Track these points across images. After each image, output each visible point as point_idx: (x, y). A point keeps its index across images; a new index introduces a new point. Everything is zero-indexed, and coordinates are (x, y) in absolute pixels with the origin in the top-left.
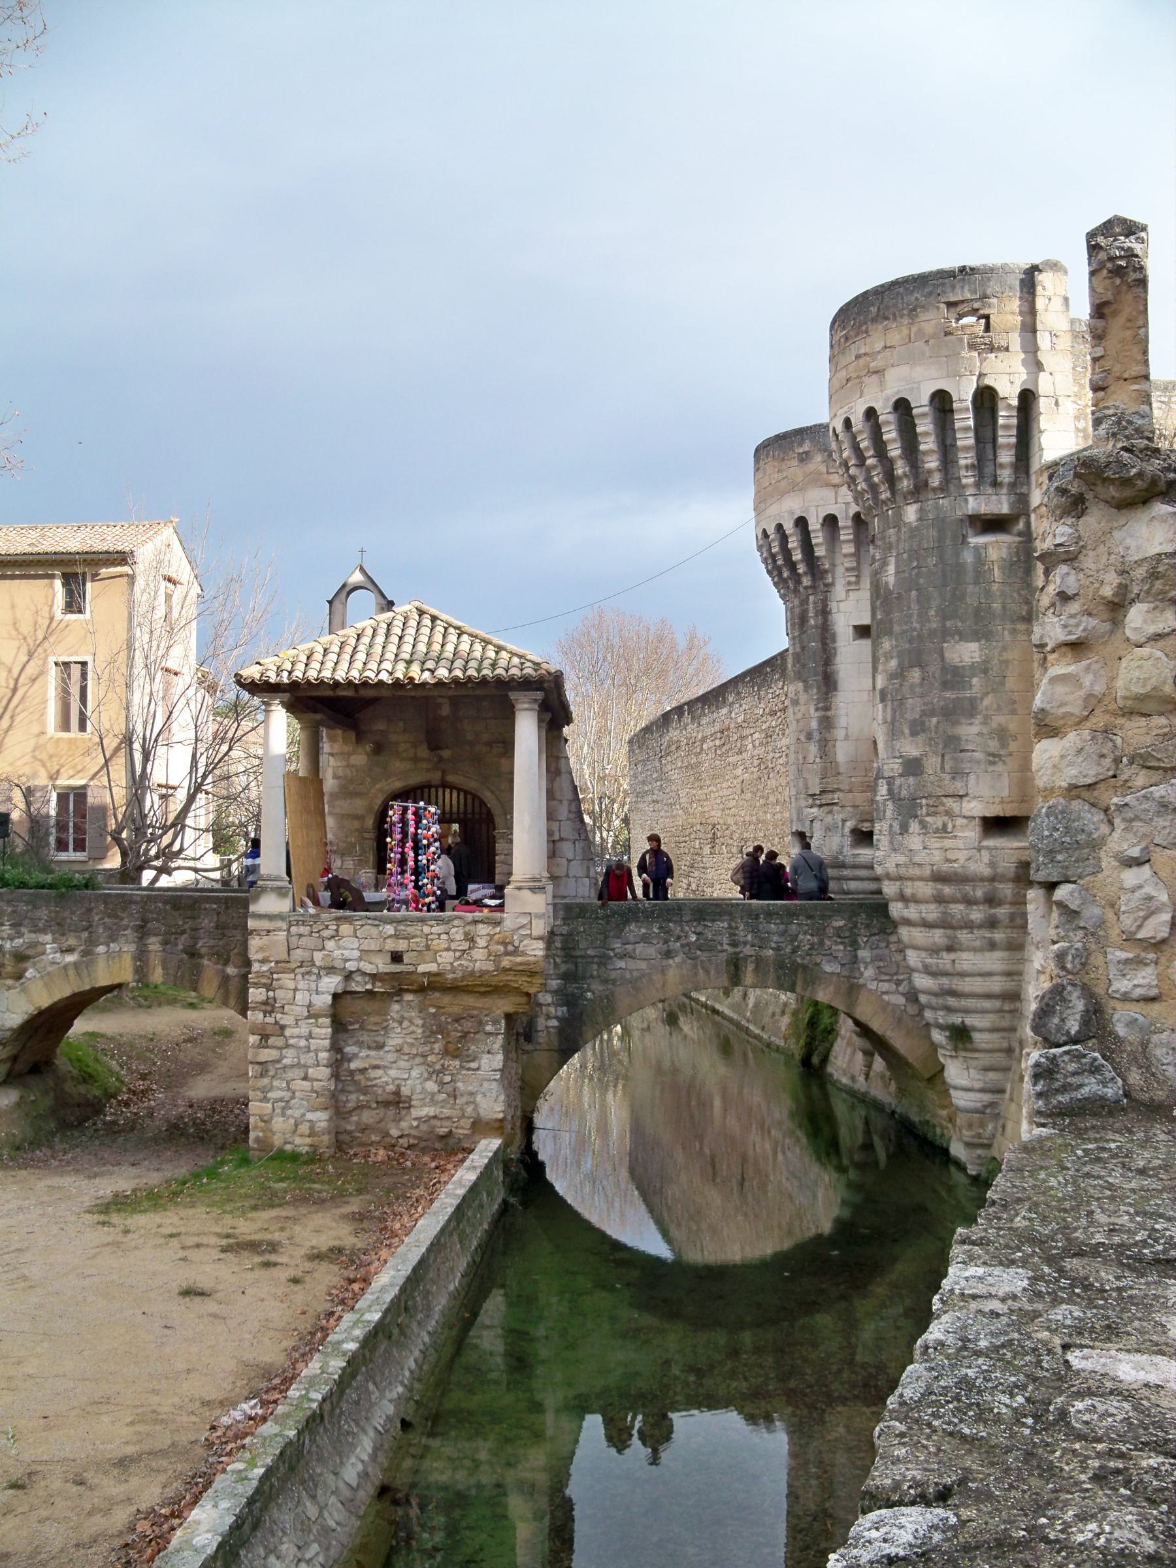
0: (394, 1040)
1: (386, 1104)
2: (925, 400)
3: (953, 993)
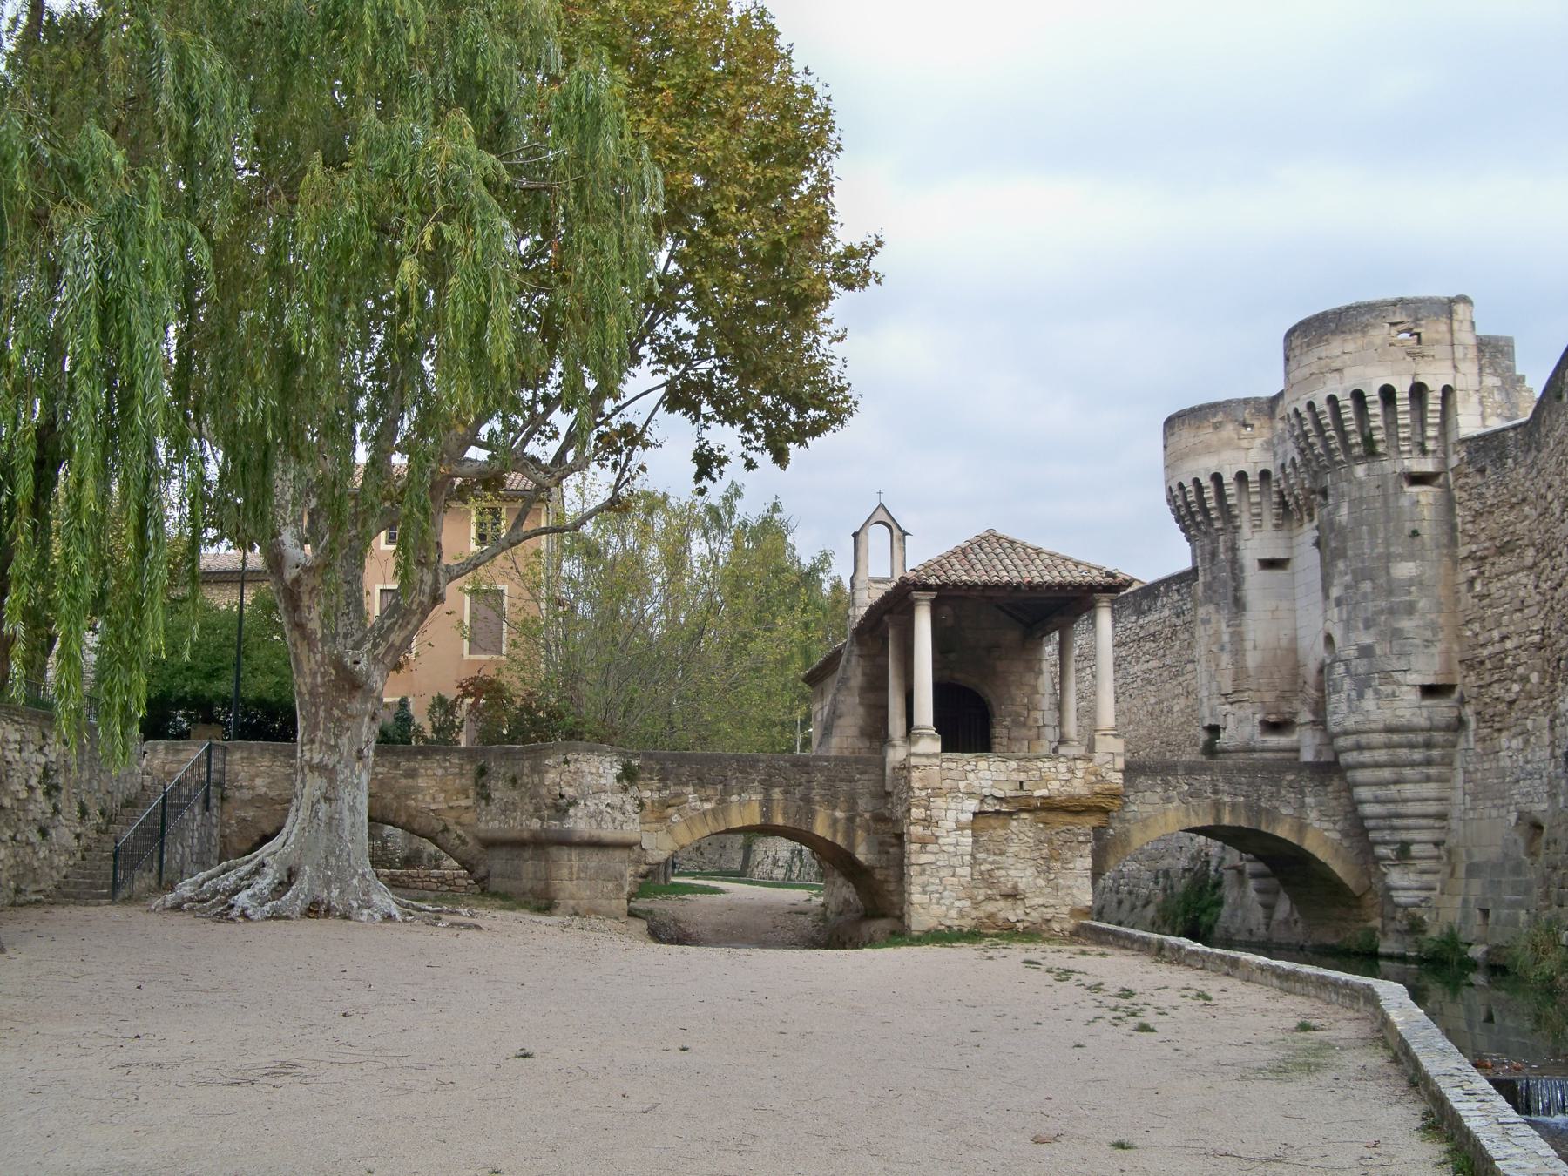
0: (1013, 849)
1: (1006, 896)
2: (1376, 391)
3: (1399, 816)
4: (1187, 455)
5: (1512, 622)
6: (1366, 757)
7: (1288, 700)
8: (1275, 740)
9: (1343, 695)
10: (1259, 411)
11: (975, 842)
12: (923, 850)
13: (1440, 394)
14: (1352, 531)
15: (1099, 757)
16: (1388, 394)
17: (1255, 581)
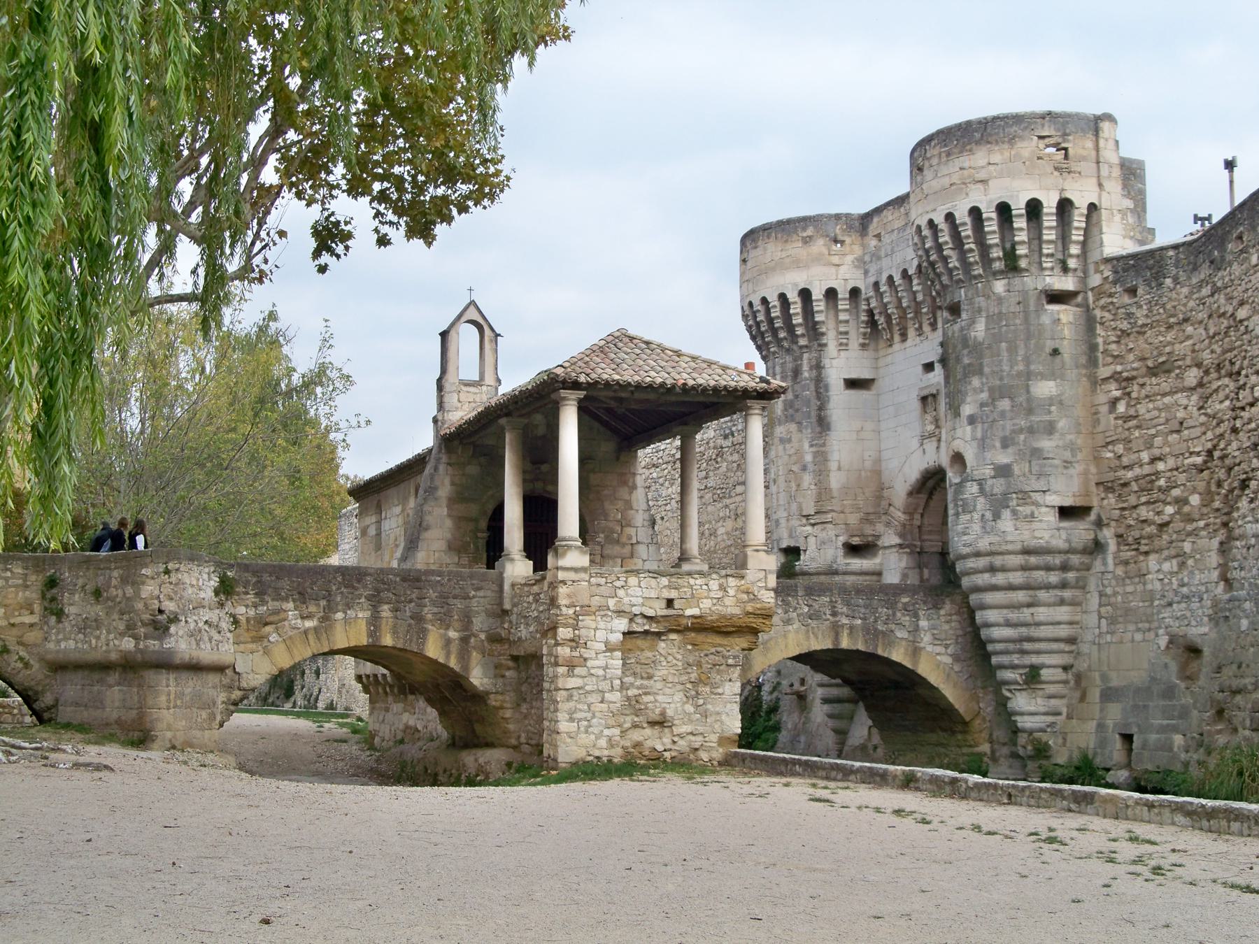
0: (661, 672)
1: (653, 724)
2: (1023, 205)
3: (1030, 639)
4: (773, 269)
5: (1166, 443)
6: (1000, 579)
7: (871, 522)
8: (857, 563)
9: (976, 516)
10: (850, 227)
11: (624, 665)
12: (571, 674)
13: (1085, 212)
14: (990, 347)
15: (752, 574)
16: (1034, 208)
17: (839, 398)
